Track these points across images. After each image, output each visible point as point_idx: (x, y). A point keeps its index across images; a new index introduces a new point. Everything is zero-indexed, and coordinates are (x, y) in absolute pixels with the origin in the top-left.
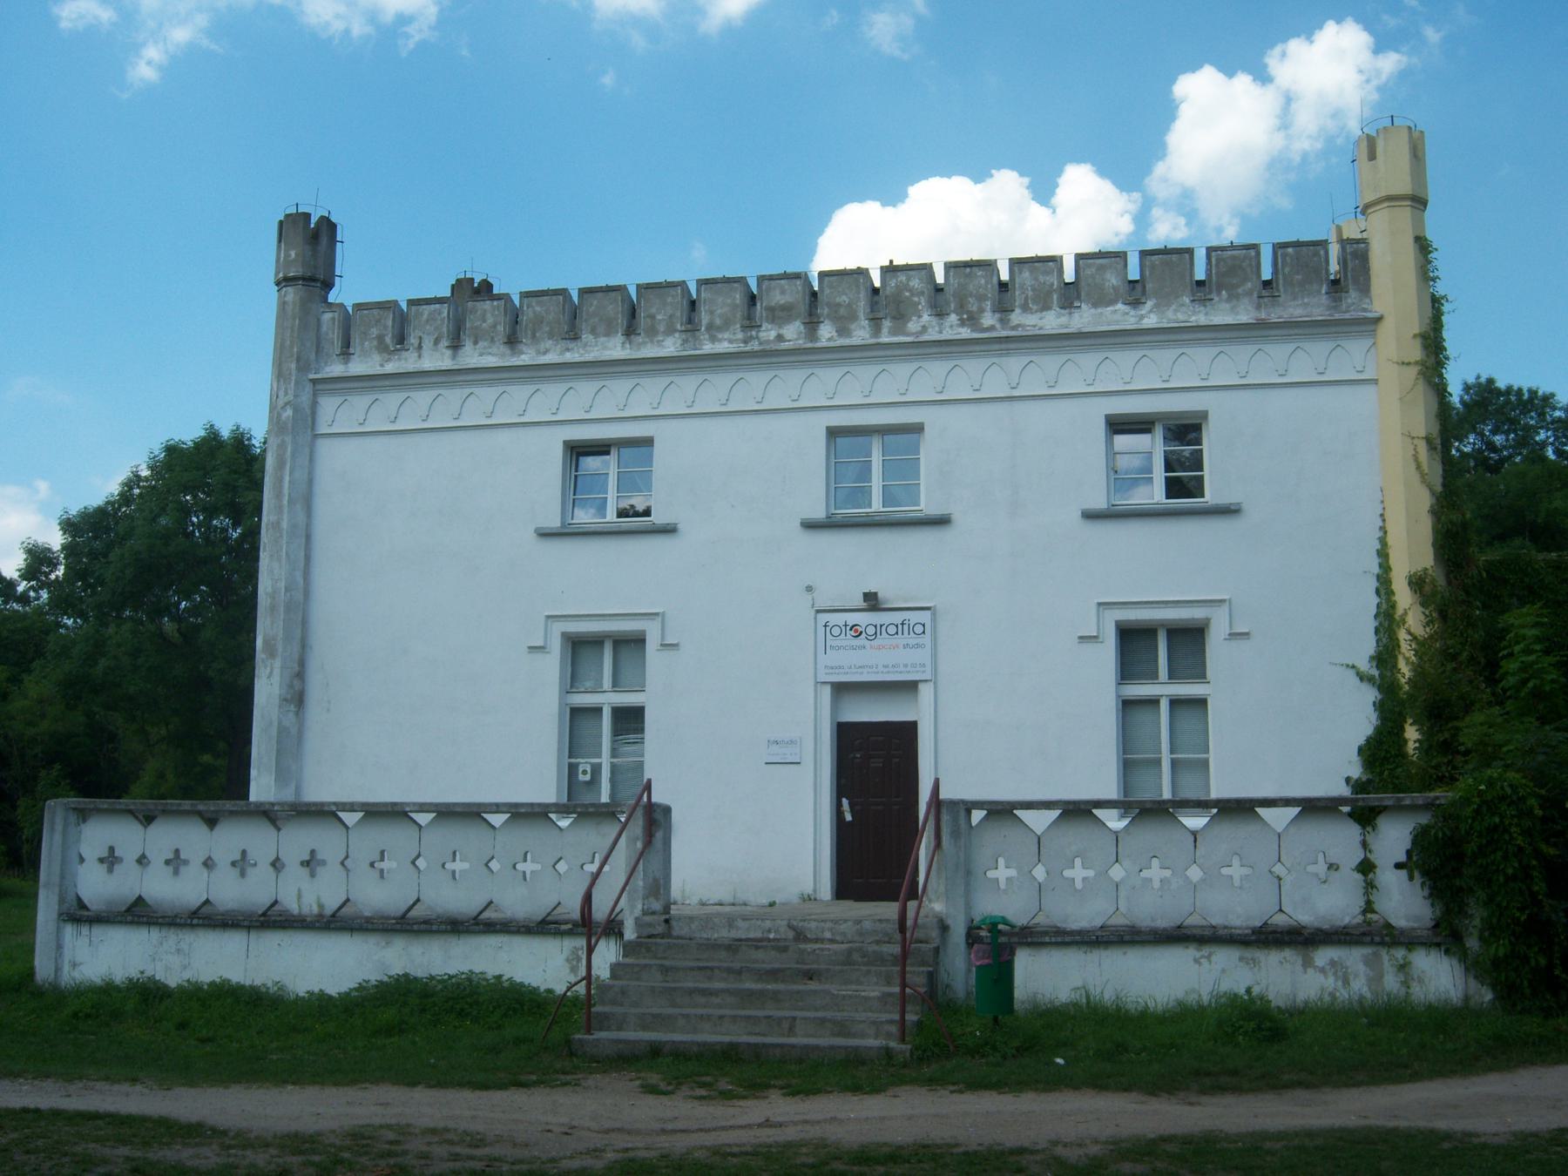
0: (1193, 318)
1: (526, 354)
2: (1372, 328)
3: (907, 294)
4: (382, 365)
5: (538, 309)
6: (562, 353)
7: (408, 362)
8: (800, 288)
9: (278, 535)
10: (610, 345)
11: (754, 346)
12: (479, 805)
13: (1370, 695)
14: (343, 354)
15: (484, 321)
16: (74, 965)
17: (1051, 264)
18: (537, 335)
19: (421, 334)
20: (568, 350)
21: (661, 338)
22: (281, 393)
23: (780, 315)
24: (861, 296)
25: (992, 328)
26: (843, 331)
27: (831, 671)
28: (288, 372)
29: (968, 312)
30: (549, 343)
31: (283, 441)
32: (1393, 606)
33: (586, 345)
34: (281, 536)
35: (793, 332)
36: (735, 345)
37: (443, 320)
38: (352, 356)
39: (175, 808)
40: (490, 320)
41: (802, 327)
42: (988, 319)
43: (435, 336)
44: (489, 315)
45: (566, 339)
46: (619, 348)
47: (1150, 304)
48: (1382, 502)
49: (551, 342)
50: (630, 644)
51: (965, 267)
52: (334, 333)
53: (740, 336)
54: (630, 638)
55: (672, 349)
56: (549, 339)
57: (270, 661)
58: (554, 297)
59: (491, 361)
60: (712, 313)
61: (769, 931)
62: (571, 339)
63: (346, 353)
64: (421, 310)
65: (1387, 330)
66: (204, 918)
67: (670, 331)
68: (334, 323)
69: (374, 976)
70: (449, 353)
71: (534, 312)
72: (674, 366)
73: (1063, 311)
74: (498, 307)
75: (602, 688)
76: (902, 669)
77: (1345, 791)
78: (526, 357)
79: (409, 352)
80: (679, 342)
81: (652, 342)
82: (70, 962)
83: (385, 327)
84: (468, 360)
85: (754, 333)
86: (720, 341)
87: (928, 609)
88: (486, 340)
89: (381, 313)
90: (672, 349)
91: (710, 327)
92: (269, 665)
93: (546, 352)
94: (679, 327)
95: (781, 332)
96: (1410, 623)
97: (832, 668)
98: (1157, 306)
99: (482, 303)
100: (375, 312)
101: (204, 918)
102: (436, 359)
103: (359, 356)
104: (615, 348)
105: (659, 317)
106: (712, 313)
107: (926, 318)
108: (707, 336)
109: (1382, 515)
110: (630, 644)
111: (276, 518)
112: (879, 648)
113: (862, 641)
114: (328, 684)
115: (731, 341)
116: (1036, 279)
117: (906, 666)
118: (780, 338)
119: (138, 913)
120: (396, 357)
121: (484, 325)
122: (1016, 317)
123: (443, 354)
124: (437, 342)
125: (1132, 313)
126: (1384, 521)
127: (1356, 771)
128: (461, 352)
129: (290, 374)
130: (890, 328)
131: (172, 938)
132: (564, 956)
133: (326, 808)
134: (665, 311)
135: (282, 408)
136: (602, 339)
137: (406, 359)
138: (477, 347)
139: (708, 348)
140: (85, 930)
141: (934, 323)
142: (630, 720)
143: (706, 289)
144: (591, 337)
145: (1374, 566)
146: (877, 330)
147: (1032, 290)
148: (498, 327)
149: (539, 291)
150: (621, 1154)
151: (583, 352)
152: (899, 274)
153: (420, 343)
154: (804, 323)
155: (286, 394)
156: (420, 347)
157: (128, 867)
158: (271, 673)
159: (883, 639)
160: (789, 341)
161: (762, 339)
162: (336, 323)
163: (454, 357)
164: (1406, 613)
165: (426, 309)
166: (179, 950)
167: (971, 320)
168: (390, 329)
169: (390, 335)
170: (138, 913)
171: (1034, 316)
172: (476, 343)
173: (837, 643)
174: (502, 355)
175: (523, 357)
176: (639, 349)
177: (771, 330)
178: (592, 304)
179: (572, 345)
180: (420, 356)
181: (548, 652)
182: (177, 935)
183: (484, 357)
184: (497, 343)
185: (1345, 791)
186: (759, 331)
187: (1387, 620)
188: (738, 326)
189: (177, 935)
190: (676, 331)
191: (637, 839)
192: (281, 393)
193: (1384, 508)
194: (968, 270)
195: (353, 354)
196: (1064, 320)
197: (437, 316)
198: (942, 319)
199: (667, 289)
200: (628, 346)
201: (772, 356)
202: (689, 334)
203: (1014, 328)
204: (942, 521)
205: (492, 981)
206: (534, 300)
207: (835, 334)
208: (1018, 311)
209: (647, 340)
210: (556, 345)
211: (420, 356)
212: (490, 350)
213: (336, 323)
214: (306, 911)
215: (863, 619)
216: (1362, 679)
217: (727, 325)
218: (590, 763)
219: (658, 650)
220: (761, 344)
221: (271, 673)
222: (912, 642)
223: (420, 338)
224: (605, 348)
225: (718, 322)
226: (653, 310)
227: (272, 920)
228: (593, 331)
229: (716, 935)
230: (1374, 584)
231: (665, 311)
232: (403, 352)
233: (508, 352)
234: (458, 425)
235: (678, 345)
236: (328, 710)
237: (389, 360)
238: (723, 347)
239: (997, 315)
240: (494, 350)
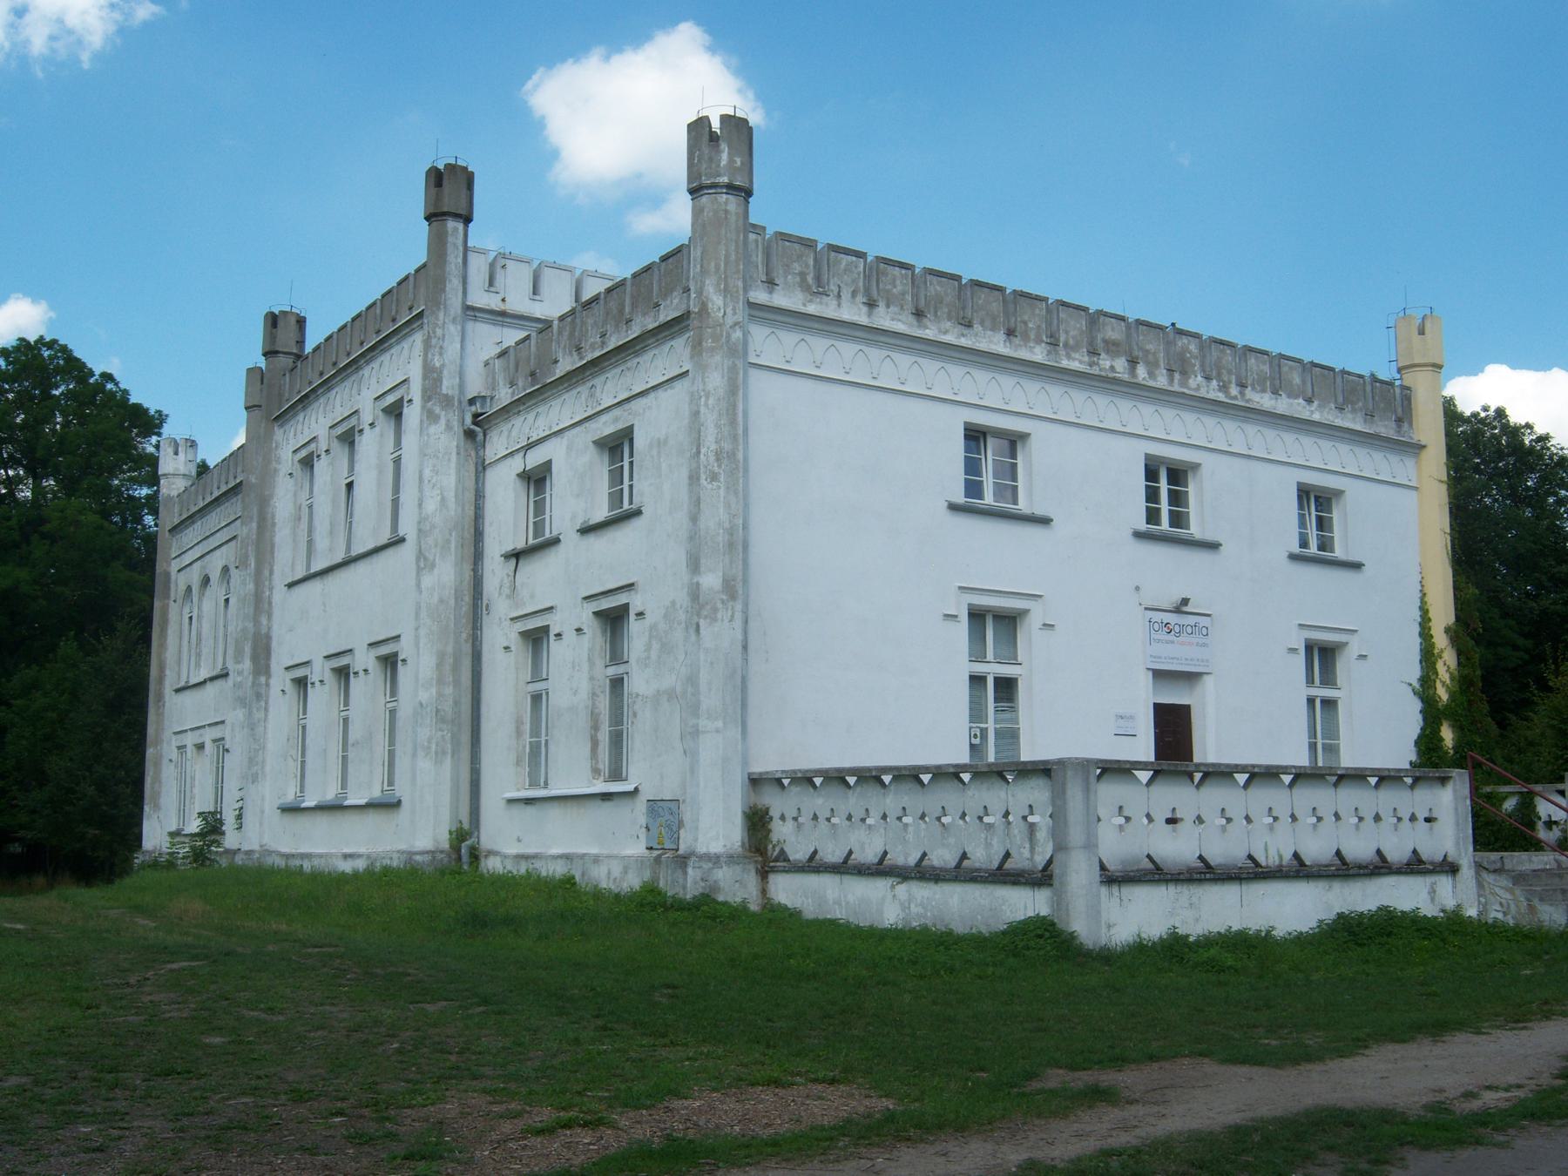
0: (1336, 421)
1: (930, 329)
2: (1417, 451)
3: (1188, 355)
4: (804, 305)
5: (938, 288)
6: (958, 337)
7: (827, 308)
8: (1124, 328)
9: (734, 466)
10: (995, 340)
11: (1095, 371)
12: (1278, 767)
13: (1417, 705)
14: (769, 283)
15: (895, 287)
16: (1109, 927)
17: (1266, 356)
18: (939, 313)
19: (839, 283)
20: (963, 335)
21: (1032, 345)
22: (729, 311)
23: (1112, 348)
24: (1161, 347)
25: (1235, 398)
26: (1151, 375)
27: (1154, 660)
28: (735, 289)
29: (1224, 382)
30: (948, 324)
31: (735, 365)
32: (1432, 646)
33: (976, 335)
34: (737, 468)
35: (1121, 364)
36: (1082, 366)
37: (859, 274)
38: (776, 287)
39: (1172, 768)
40: (899, 288)
41: (1126, 364)
42: (1234, 391)
43: (852, 289)
44: (898, 282)
45: (961, 324)
46: (1002, 345)
47: (1316, 403)
48: (1421, 573)
49: (949, 323)
50: (1009, 621)
51: (1221, 343)
52: (757, 256)
53: (1086, 359)
54: (1004, 614)
55: (1040, 357)
56: (948, 320)
57: (731, 603)
58: (951, 281)
59: (900, 327)
60: (1067, 332)
61: (1546, 864)
62: (965, 326)
63: (771, 283)
64: (839, 258)
65: (1426, 455)
66: (1205, 873)
67: (1039, 341)
68: (757, 246)
69: (1329, 916)
70: (865, 309)
71: (936, 290)
72: (957, 355)
73: (1273, 396)
74: (906, 275)
75: (985, 657)
76: (1183, 662)
77: (1408, 767)
78: (930, 333)
79: (829, 298)
80: (1045, 352)
81: (1026, 346)
82: (1105, 923)
83: (807, 266)
84: (882, 322)
85: (1095, 359)
86: (1074, 359)
87: (1209, 615)
88: (896, 306)
89: (803, 249)
90: (1040, 357)
91: (1066, 345)
92: (730, 607)
93: (946, 332)
94: (1044, 338)
95: (1114, 364)
96: (1447, 658)
97: (1155, 657)
98: (1319, 406)
99: (892, 267)
100: (797, 246)
101: (1205, 873)
102: (902, 324)
103: (783, 289)
104: (852, 312)
105: (1030, 325)
106: (1067, 332)
107: (1199, 378)
108: (1064, 353)
109: (1421, 582)
110: (1009, 621)
111: (731, 447)
112: (1183, 644)
113: (1171, 637)
114: (765, 634)
115: (1081, 362)
116: (1258, 366)
117: (1186, 659)
118: (1112, 368)
119: (1155, 873)
120: (818, 300)
121: (895, 290)
122: (1249, 393)
123: (859, 309)
124: (854, 294)
125: (1308, 407)
126: (1422, 586)
127: (1413, 757)
128: (876, 310)
129: (737, 292)
130: (1179, 380)
131: (1185, 893)
132: (1427, 891)
133: (1271, 771)
134: (1073, 328)
135: (731, 327)
136: (989, 333)
137: (827, 304)
138: (889, 310)
139: (1065, 363)
140: (1115, 889)
141: (1204, 384)
142: (1006, 688)
143: (1062, 310)
144: (981, 328)
145: (1417, 614)
146: (1171, 380)
147: (1257, 374)
148: (907, 296)
149: (939, 271)
150: (1360, 1052)
151: (974, 340)
152: (1184, 337)
153: (839, 292)
154: (1128, 361)
155: (735, 314)
156: (839, 296)
157: (1186, 826)
158: (732, 616)
159: (1184, 638)
160: (1119, 373)
161: (1102, 367)
162: (760, 246)
163: (870, 315)
164: (1442, 651)
165: (846, 260)
166: (1191, 904)
167: (1224, 388)
168: (812, 267)
169: (812, 275)
170: (1155, 873)
171: (1257, 395)
172: (888, 306)
173: (1156, 637)
174: (911, 325)
175: (927, 331)
176: (1016, 351)
177: (1107, 360)
178: (980, 298)
179: (965, 331)
180: (839, 305)
181: (959, 622)
182: (1189, 890)
183: (895, 322)
184: (906, 312)
185: (1408, 767)
186: (1099, 359)
187: (1428, 656)
188: (1085, 350)
189: (1189, 890)
190: (1043, 341)
191: (1466, 798)
192: (729, 311)
193: (1422, 578)
194: (1222, 346)
195: (777, 285)
196: (1273, 402)
197: (854, 269)
198: (1209, 382)
199: (1036, 301)
200: (1008, 344)
201: (1118, 384)
202: (1052, 346)
203: (1248, 401)
204: (1213, 546)
205: (1399, 914)
206: (935, 278)
207: (1147, 376)
208: (1249, 388)
209: (1022, 343)
210: (954, 328)
211: (839, 305)
212: (900, 317)
213: (760, 246)
214: (1271, 862)
215: (1172, 619)
216: (1415, 694)
217: (1076, 348)
218: (979, 728)
219: (1040, 629)
220: (1100, 370)
221: (732, 616)
222: (1201, 641)
223: (839, 287)
224: (991, 342)
225: (1071, 342)
226: (1026, 318)
227: (1253, 872)
228: (982, 323)
229: (1524, 868)
230: (1417, 629)
231: (1033, 320)
232: (824, 297)
233: (915, 323)
234: (876, 385)
235: (1044, 355)
236: (767, 660)
237: (811, 301)
238: (1075, 365)
239: (1238, 388)
240: (903, 317)
